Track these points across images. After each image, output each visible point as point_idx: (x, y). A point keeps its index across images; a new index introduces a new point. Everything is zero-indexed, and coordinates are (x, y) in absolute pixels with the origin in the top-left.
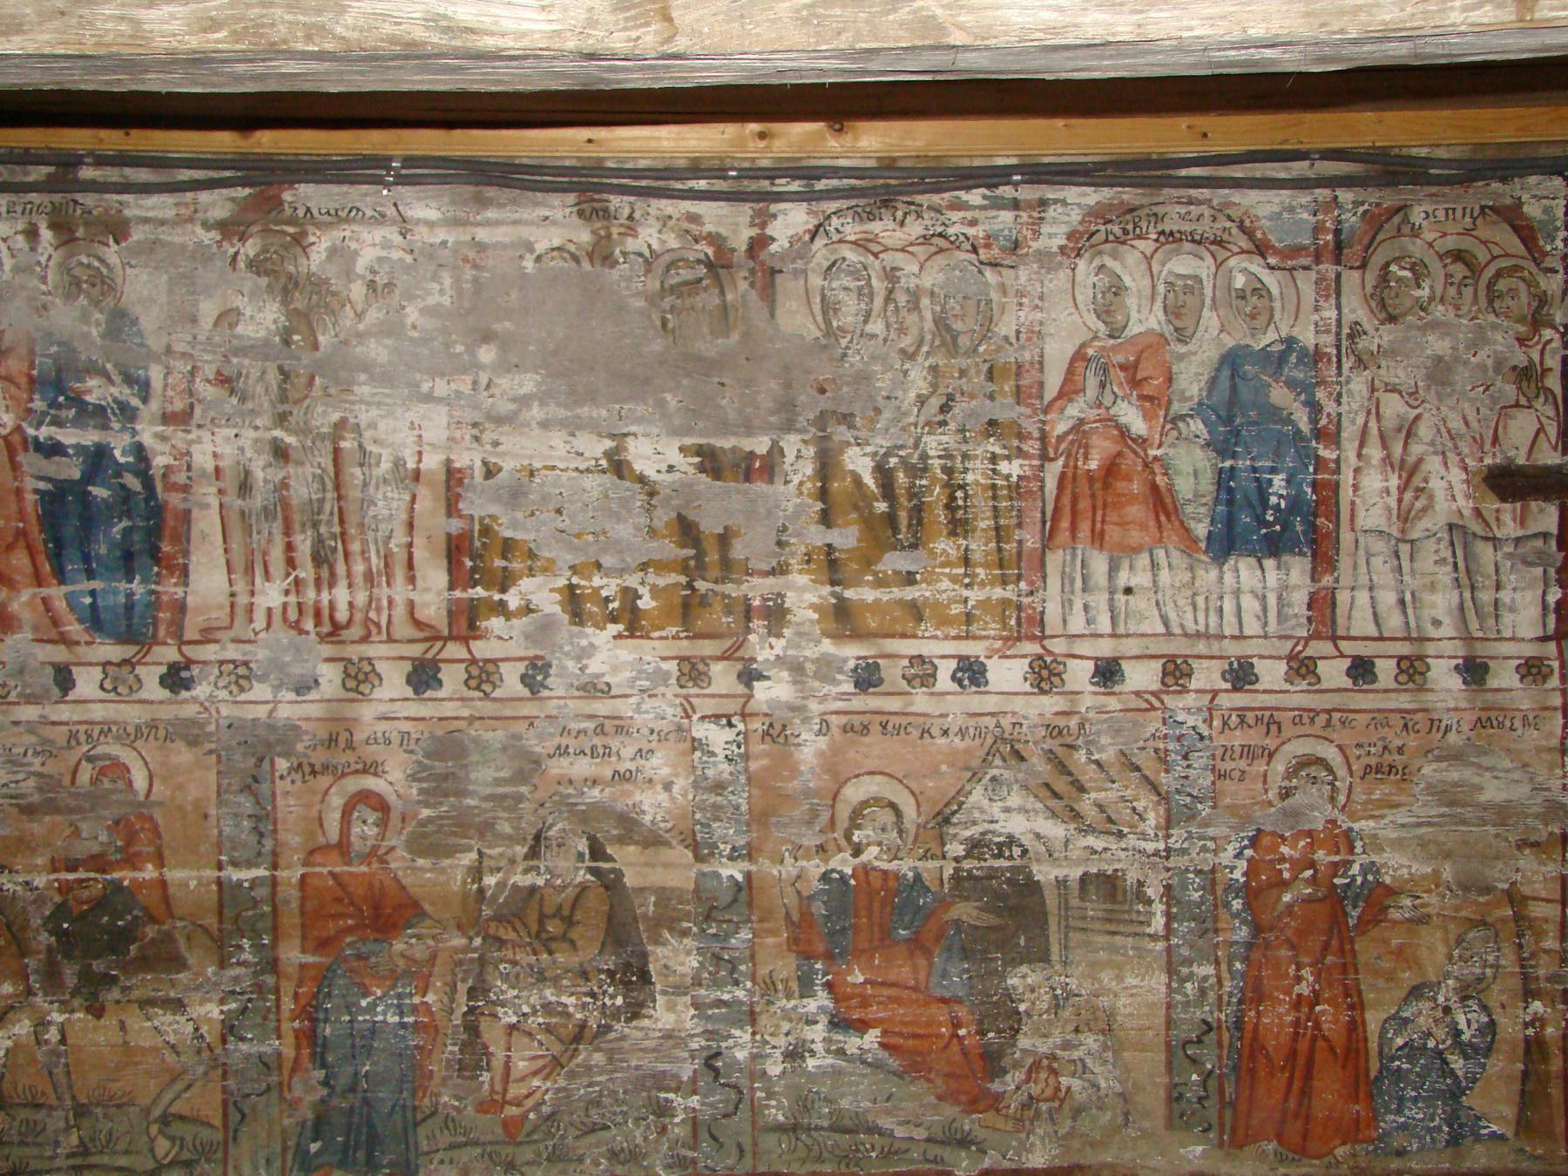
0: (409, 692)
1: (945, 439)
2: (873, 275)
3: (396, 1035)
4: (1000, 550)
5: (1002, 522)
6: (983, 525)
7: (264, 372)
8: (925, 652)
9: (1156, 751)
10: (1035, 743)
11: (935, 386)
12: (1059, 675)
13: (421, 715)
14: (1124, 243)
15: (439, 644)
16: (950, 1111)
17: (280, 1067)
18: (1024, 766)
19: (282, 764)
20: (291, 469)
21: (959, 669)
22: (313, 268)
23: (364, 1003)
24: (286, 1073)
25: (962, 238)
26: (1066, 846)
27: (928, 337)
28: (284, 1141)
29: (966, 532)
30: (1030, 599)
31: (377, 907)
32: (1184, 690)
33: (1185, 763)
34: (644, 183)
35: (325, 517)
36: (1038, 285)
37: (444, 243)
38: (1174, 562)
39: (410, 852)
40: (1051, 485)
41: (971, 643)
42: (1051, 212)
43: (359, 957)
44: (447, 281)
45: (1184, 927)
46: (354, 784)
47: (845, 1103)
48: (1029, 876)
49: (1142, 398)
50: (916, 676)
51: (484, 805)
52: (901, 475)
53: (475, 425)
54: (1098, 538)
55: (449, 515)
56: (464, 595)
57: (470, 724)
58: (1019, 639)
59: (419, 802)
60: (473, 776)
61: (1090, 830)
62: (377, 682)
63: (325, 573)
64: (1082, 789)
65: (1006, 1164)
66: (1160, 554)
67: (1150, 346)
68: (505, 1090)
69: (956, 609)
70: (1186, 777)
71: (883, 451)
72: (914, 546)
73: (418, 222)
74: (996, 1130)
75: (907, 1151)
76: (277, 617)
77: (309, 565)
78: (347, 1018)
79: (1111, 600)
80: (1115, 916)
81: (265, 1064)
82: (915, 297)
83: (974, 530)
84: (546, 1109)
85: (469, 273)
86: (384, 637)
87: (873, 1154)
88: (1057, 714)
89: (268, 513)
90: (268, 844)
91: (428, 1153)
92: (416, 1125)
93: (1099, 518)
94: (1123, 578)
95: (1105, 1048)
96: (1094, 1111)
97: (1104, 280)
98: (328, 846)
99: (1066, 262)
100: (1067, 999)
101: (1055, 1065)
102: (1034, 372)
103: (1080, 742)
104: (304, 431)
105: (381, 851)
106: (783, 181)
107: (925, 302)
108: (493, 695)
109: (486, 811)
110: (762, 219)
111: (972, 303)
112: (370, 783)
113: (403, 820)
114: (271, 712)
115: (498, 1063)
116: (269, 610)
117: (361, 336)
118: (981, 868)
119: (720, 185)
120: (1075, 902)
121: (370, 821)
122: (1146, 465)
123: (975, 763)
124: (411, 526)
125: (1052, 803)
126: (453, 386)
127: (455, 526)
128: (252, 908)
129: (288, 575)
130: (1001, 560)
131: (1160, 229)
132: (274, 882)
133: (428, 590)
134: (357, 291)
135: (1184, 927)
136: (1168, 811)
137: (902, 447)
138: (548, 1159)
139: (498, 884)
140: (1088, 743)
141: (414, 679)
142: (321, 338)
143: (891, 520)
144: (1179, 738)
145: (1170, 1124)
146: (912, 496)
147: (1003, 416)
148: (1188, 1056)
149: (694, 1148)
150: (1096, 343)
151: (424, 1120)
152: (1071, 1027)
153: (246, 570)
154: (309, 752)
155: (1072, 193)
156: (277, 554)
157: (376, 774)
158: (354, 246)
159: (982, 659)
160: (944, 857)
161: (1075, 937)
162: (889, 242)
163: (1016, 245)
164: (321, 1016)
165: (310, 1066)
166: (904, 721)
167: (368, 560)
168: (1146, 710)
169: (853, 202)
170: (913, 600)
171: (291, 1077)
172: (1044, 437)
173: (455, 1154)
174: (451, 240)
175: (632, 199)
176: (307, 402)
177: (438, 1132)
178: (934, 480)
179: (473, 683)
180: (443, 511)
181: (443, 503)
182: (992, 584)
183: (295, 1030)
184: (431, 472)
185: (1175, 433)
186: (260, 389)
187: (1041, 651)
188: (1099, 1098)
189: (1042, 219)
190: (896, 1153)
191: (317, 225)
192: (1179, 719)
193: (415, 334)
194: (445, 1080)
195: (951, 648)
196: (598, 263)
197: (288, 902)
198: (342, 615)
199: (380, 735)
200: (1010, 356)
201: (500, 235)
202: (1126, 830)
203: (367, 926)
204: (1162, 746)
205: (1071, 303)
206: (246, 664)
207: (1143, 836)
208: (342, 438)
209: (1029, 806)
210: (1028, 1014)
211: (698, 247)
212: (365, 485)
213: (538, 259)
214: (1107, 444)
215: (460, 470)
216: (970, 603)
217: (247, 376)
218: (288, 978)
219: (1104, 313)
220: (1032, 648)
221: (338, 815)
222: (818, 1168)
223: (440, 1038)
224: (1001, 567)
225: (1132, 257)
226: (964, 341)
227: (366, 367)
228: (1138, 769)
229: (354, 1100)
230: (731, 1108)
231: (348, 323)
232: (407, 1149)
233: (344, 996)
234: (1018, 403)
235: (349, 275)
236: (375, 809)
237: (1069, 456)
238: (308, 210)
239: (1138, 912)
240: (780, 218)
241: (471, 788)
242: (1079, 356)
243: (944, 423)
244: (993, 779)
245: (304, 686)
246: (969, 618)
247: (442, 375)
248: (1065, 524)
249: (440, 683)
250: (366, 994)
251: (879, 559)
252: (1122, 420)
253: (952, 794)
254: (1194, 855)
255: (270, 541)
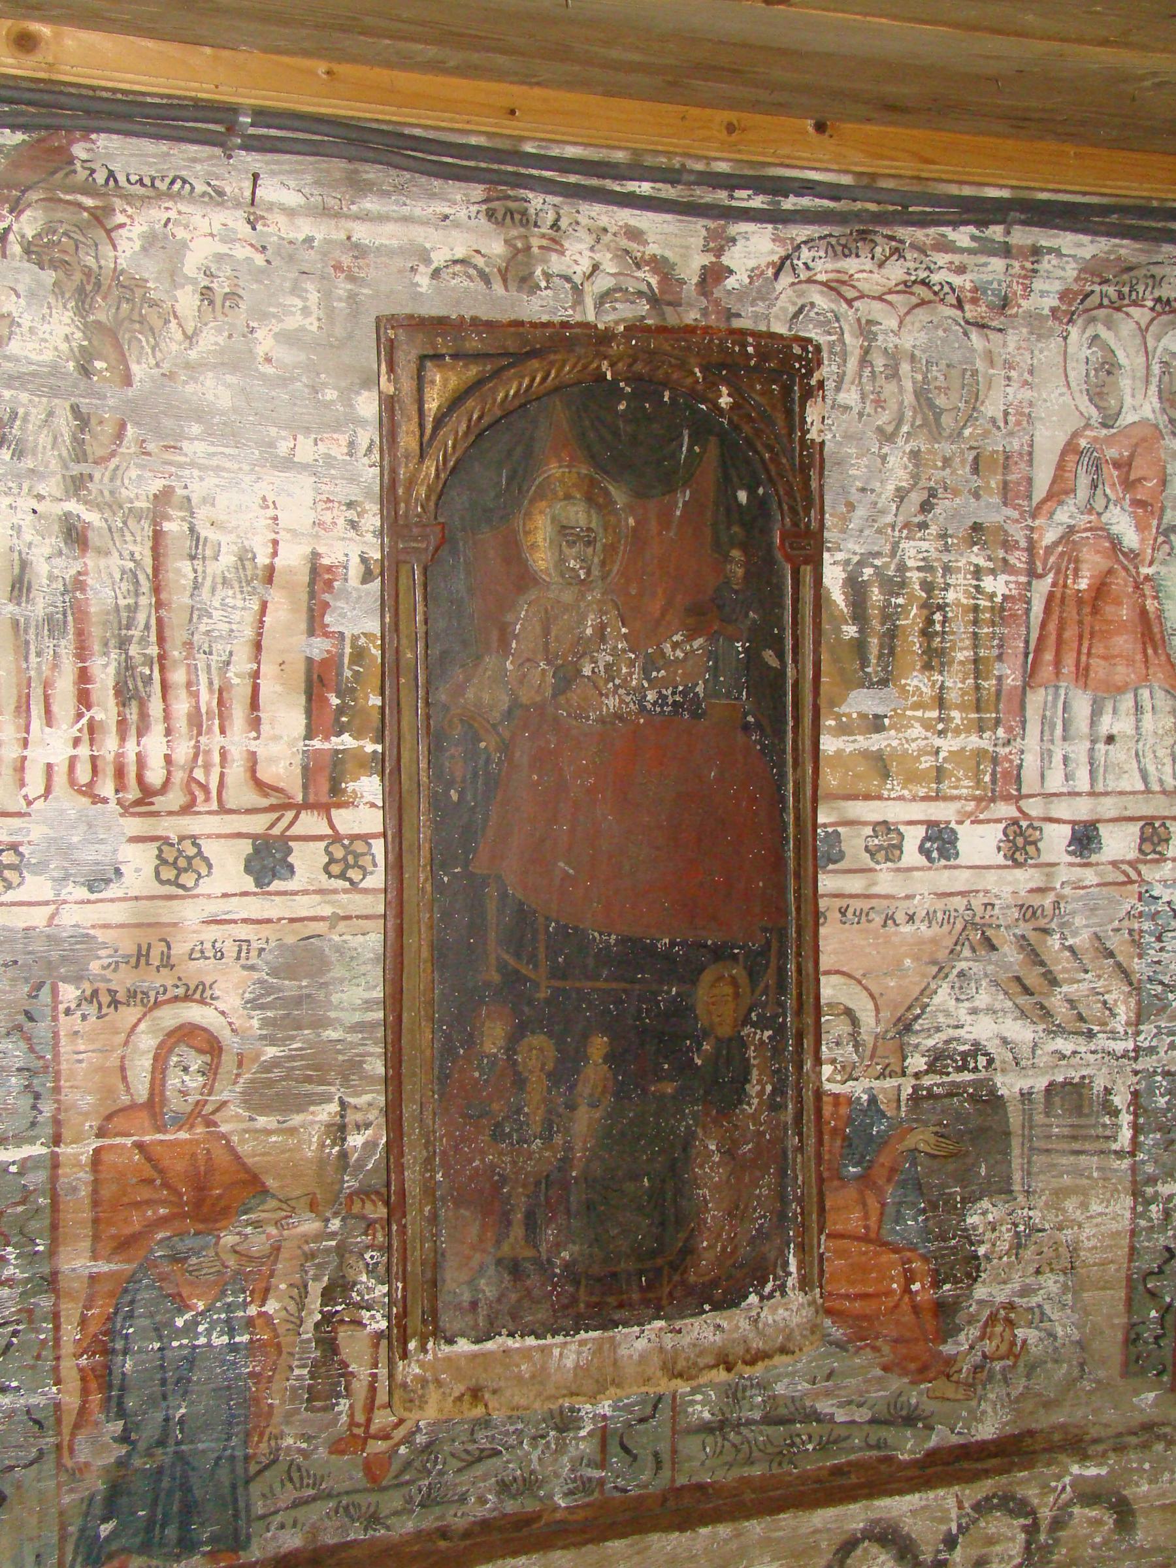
0: (249, 883)
1: (925, 545)
2: (846, 328)
3: (223, 1362)
4: (978, 688)
5: (982, 653)
6: (960, 656)
7: (51, 414)
8: (890, 818)
9: (1131, 931)
10: (1008, 927)
11: (915, 477)
12: (1034, 843)
13: (266, 915)
14: (1118, 309)
15: (290, 815)
16: (897, 1383)
17: (59, 1421)
18: (994, 956)
19: (69, 993)
20: (90, 560)
21: (927, 838)
22: (123, 263)
23: (180, 1322)
24: (66, 1430)
25: (947, 289)
26: (1033, 1052)
27: (909, 414)
28: (63, 1527)
29: (942, 664)
30: (1007, 750)
31: (200, 1185)
32: (1162, 859)
33: (1158, 946)
34: (573, 179)
35: (136, 633)
36: (1028, 355)
37: (309, 240)
38: (1158, 703)
39: (248, 1109)
40: (1037, 608)
41: (941, 804)
42: (1047, 263)
43: (175, 1259)
44: (314, 297)
45: (1149, 1140)
46: (171, 1016)
47: (780, 1389)
48: (993, 1091)
49: (1138, 503)
50: (880, 848)
51: (350, 1038)
52: (876, 590)
53: (350, 505)
54: (1082, 674)
55: (311, 632)
56: (327, 746)
57: (332, 927)
58: (993, 800)
59: (263, 1038)
60: (335, 998)
61: (1059, 1031)
62: (204, 871)
63: (133, 715)
64: (1054, 982)
65: (954, 1439)
66: (1145, 693)
67: (1144, 440)
68: (369, 1421)
69: (926, 763)
70: (1159, 962)
71: (856, 559)
72: (884, 683)
73: (270, 207)
74: (945, 1399)
75: (848, 1437)
76: (60, 778)
77: (111, 702)
78: (157, 1345)
79: (1092, 750)
80: (1084, 1132)
81: (37, 1422)
82: (894, 358)
83: (951, 663)
84: (420, 1439)
85: (343, 287)
86: (214, 806)
87: (810, 1447)
88: (1031, 891)
89: (53, 626)
90: (47, 1109)
91: (263, 1517)
92: (248, 1481)
93: (1085, 650)
94: (1106, 724)
95: (1065, 1289)
96: (1049, 1365)
97: (1096, 355)
98: (133, 1107)
99: (1058, 328)
100: (1029, 1235)
101: (1012, 1315)
102: (1023, 465)
103: (1053, 925)
104: (112, 505)
105: (209, 1108)
106: (743, 194)
107: (905, 367)
108: (362, 885)
109: (353, 1045)
110: (719, 243)
111: (954, 373)
112: (195, 1013)
113: (240, 1064)
114: (52, 917)
115: (360, 1387)
116: (49, 766)
117: (193, 369)
118: (942, 1084)
119: (668, 192)
120: (1039, 1118)
121: (194, 1068)
122: (1137, 587)
123: (942, 955)
124: (258, 646)
125: (1022, 1000)
126: (322, 448)
127: (319, 648)
128: (23, 1202)
129: (80, 716)
130: (978, 700)
131: (1156, 294)
132: (55, 1163)
133: (276, 738)
134: (187, 301)
135: (1149, 1140)
136: (1139, 1003)
137: (878, 554)
138: (422, 1505)
139: (366, 1144)
140: (1062, 925)
141: (256, 865)
142: (135, 368)
143: (860, 646)
144: (1154, 916)
145: (1125, 1374)
146: (886, 617)
147: (990, 518)
148: (1149, 1291)
149: (602, 1465)
150: (1088, 433)
151: (259, 1472)
152: (1031, 1270)
153: (18, 708)
154: (108, 973)
155: (1067, 241)
156: (65, 686)
157: (202, 1001)
158: (181, 233)
159: (953, 825)
160: (904, 1074)
161: (1039, 1160)
162: (864, 287)
163: (1005, 303)
164: (119, 1345)
165: (103, 1417)
166: (865, 905)
167: (195, 695)
168: (1123, 884)
169: (826, 230)
170: (880, 750)
171: (73, 1435)
172: (1031, 548)
173: (300, 1513)
174: (319, 237)
175: (557, 200)
176: (114, 462)
177: (277, 1486)
178: (911, 598)
179: (336, 869)
180: (303, 626)
181: (304, 616)
182: (968, 731)
183: (81, 1370)
184: (291, 571)
185: (1166, 547)
186: (44, 439)
187: (1017, 814)
188: (1056, 1349)
189: (1035, 271)
190: (835, 1442)
191: (128, 198)
192: (1155, 893)
193: (269, 370)
194: (288, 1417)
195: (919, 811)
196: (513, 286)
197: (75, 1189)
198: (155, 776)
199: (207, 945)
200: (996, 444)
201: (386, 235)
202: (1096, 1028)
203: (184, 1216)
204: (1136, 926)
205: (1062, 382)
206: (14, 847)
207: (1113, 1035)
208: (168, 518)
209: (998, 1006)
210: (987, 1257)
211: (640, 274)
212: (196, 586)
213: (436, 274)
214: (1098, 558)
215: (329, 569)
216: (942, 755)
217: (25, 420)
218: (71, 1296)
219: (1097, 395)
220: (1006, 810)
221: (147, 1062)
222: (747, 1471)
223: (283, 1361)
224: (978, 709)
225: (1127, 328)
226: (946, 420)
227: (200, 414)
228: (1111, 955)
229: (164, 1456)
230: (648, 1410)
231: (174, 347)
232: (236, 1516)
233: (152, 1315)
234: (1005, 504)
235: (174, 276)
236: (201, 1051)
237: (1058, 573)
238: (111, 174)
239: (1104, 1126)
240: (740, 243)
241: (332, 1014)
242: (1070, 448)
243: (923, 526)
244: (961, 974)
245: (98, 880)
246: (940, 774)
247: (307, 430)
248: (1049, 656)
249: (291, 869)
250: (180, 1312)
251: (843, 699)
252: (1115, 529)
253: (916, 994)
254: (1162, 1054)
255: (55, 666)
